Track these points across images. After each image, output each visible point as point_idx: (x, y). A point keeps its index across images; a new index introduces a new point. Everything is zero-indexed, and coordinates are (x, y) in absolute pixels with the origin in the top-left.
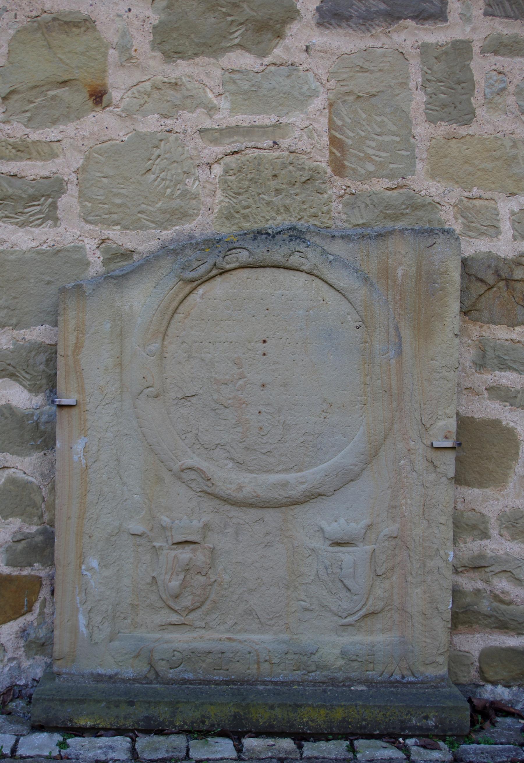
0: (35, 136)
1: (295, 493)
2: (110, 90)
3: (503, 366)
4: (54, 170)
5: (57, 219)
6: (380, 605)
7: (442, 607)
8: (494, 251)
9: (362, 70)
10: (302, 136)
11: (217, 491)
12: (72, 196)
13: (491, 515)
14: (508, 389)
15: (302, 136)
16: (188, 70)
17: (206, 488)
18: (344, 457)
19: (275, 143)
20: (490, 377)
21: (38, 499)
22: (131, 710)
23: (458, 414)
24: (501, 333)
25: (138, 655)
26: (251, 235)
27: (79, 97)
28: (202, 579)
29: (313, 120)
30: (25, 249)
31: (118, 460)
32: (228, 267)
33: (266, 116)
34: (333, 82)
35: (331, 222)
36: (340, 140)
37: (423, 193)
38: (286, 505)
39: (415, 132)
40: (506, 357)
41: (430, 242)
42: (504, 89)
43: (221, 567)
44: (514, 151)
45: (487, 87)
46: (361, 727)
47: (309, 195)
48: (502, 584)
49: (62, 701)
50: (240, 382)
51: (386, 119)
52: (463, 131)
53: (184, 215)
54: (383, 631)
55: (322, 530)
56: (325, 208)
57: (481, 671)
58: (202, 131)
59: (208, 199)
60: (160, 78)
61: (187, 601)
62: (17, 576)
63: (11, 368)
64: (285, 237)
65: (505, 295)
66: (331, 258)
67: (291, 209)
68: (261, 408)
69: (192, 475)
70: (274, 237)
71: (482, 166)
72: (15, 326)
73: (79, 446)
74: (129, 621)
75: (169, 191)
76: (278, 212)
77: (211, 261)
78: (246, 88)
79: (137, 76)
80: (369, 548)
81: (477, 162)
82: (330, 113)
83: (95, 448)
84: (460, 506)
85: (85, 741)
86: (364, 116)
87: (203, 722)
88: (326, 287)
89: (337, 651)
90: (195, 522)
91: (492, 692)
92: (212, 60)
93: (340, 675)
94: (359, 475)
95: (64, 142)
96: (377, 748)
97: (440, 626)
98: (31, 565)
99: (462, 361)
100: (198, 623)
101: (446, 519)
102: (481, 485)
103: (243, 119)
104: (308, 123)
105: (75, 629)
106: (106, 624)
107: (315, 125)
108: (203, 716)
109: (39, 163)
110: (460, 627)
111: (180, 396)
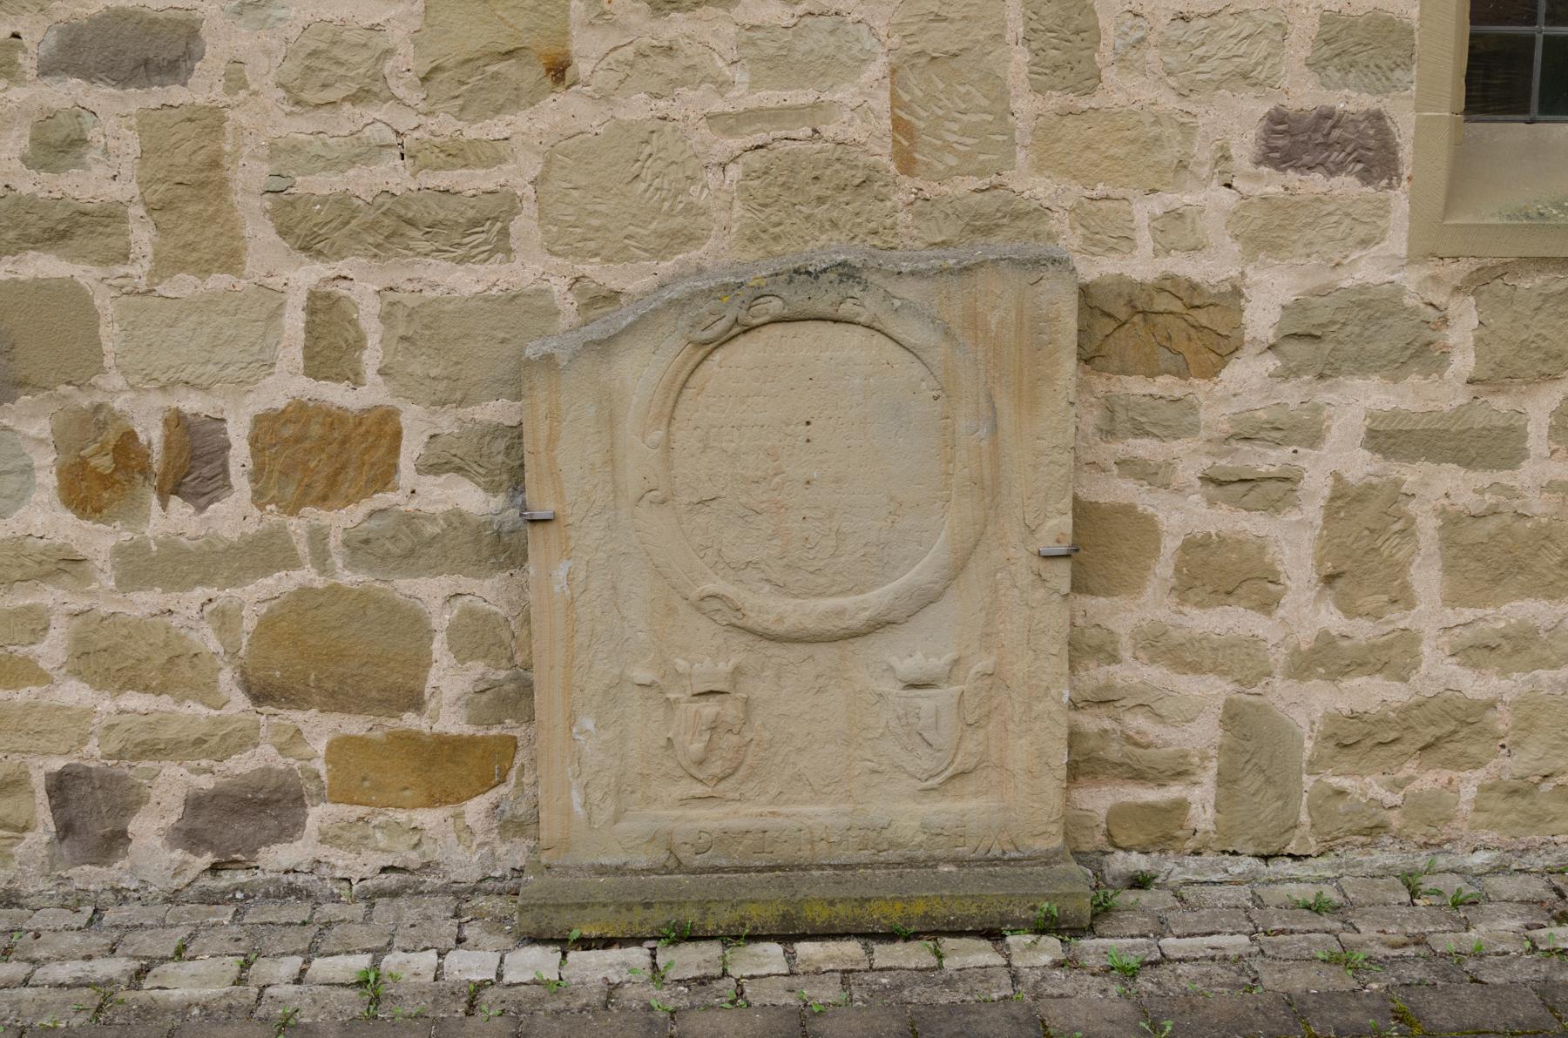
0: (472, 133)
1: (858, 621)
2: (576, 60)
3: (1140, 431)
4: (502, 181)
5: (511, 250)
6: (973, 762)
7: (1055, 763)
8: (1127, 272)
9: (938, 18)
10: (852, 119)
11: (750, 624)
12: (530, 218)
13: (1122, 632)
14: (1145, 463)
15: (852, 119)
16: (687, 28)
17: (734, 621)
18: (919, 573)
19: (815, 131)
20: (1121, 447)
21: (506, 636)
22: (647, 914)
23: (1076, 499)
24: (1136, 386)
25: (653, 839)
26: (785, 277)
27: (531, 74)
28: (734, 739)
29: (869, 95)
30: (467, 295)
31: (614, 588)
32: (755, 322)
33: (800, 91)
34: (896, 39)
35: (896, 241)
36: (908, 123)
37: (1026, 195)
38: (842, 638)
39: (1013, 107)
40: (1143, 419)
41: (1034, 277)
42: (1143, 39)
43: (758, 722)
44: (1156, 130)
45: (1119, 36)
46: (948, 923)
47: (865, 203)
48: (1137, 722)
49: (558, 906)
50: (777, 479)
51: (973, 90)
52: (1083, 103)
53: (688, 238)
54: (976, 794)
55: (891, 668)
56: (889, 222)
57: (1109, 835)
58: (710, 117)
59: (723, 214)
60: (646, 40)
61: (716, 768)
62: (483, 738)
63: (457, 460)
64: (832, 276)
65: (1142, 333)
66: (897, 303)
67: (841, 224)
68: (805, 512)
69: (716, 604)
70: (817, 278)
71: (1111, 152)
72: (461, 403)
73: (561, 573)
74: (639, 795)
75: (666, 205)
76: (822, 229)
77: (730, 316)
78: (771, 51)
79: (614, 39)
80: (956, 689)
81: (1103, 147)
82: (892, 83)
83: (582, 575)
84: (1079, 622)
85: (594, 957)
86: (941, 86)
87: (743, 925)
88: (891, 344)
89: (916, 824)
90: (721, 665)
91: (1125, 860)
92: (721, 12)
93: (921, 854)
94: (941, 594)
95: (513, 140)
96: (970, 952)
97: (1052, 784)
98: (500, 722)
99: (1081, 426)
100: (730, 795)
101: (1059, 648)
102: (1108, 593)
103: (769, 97)
104: (860, 100)
105: (568, 811)
106: (609, 801)
107: (872, 103)
108: (742, 917)
109: (481, 172)
110: (1081, 779)
111: (695, 500)
